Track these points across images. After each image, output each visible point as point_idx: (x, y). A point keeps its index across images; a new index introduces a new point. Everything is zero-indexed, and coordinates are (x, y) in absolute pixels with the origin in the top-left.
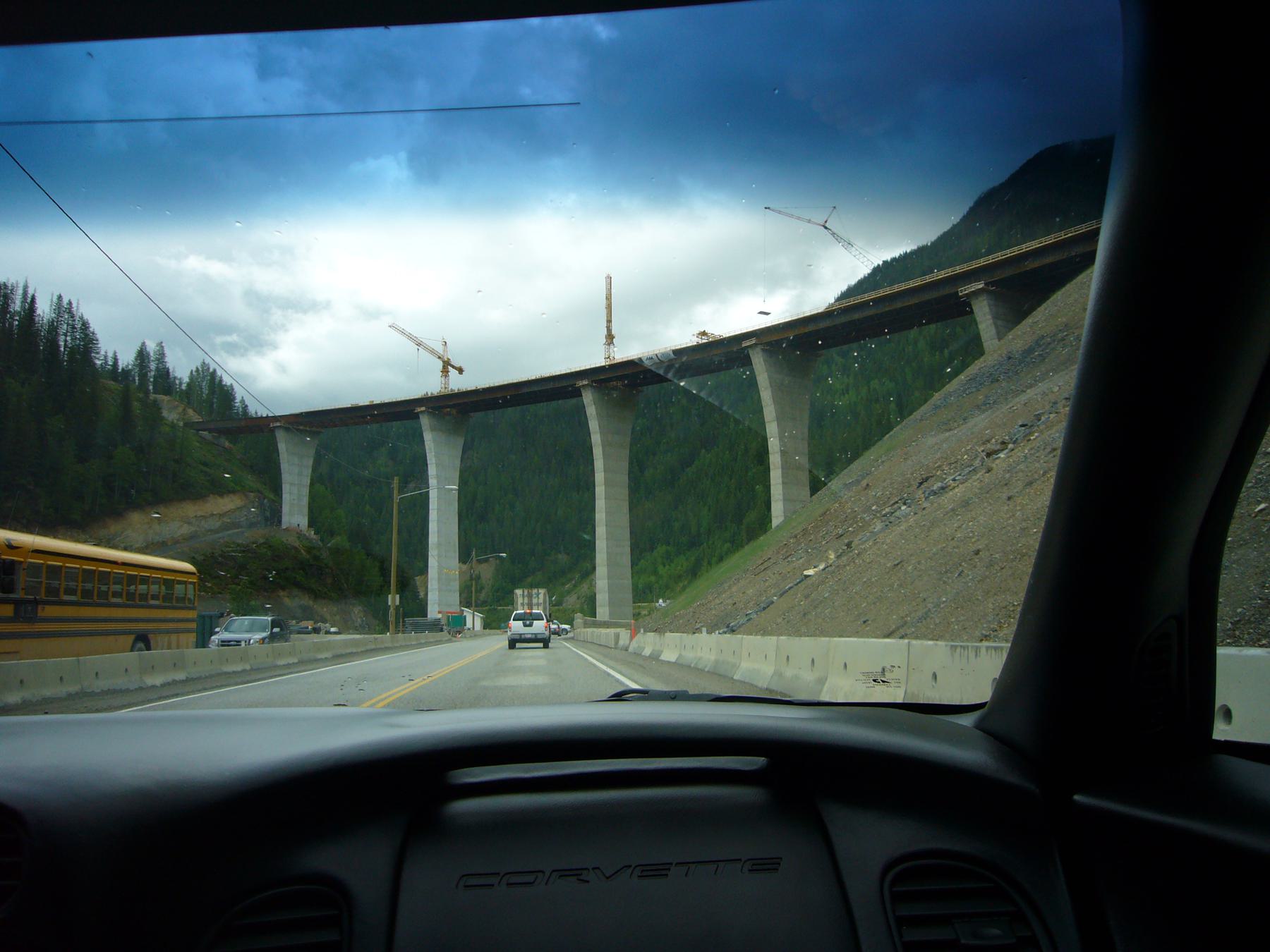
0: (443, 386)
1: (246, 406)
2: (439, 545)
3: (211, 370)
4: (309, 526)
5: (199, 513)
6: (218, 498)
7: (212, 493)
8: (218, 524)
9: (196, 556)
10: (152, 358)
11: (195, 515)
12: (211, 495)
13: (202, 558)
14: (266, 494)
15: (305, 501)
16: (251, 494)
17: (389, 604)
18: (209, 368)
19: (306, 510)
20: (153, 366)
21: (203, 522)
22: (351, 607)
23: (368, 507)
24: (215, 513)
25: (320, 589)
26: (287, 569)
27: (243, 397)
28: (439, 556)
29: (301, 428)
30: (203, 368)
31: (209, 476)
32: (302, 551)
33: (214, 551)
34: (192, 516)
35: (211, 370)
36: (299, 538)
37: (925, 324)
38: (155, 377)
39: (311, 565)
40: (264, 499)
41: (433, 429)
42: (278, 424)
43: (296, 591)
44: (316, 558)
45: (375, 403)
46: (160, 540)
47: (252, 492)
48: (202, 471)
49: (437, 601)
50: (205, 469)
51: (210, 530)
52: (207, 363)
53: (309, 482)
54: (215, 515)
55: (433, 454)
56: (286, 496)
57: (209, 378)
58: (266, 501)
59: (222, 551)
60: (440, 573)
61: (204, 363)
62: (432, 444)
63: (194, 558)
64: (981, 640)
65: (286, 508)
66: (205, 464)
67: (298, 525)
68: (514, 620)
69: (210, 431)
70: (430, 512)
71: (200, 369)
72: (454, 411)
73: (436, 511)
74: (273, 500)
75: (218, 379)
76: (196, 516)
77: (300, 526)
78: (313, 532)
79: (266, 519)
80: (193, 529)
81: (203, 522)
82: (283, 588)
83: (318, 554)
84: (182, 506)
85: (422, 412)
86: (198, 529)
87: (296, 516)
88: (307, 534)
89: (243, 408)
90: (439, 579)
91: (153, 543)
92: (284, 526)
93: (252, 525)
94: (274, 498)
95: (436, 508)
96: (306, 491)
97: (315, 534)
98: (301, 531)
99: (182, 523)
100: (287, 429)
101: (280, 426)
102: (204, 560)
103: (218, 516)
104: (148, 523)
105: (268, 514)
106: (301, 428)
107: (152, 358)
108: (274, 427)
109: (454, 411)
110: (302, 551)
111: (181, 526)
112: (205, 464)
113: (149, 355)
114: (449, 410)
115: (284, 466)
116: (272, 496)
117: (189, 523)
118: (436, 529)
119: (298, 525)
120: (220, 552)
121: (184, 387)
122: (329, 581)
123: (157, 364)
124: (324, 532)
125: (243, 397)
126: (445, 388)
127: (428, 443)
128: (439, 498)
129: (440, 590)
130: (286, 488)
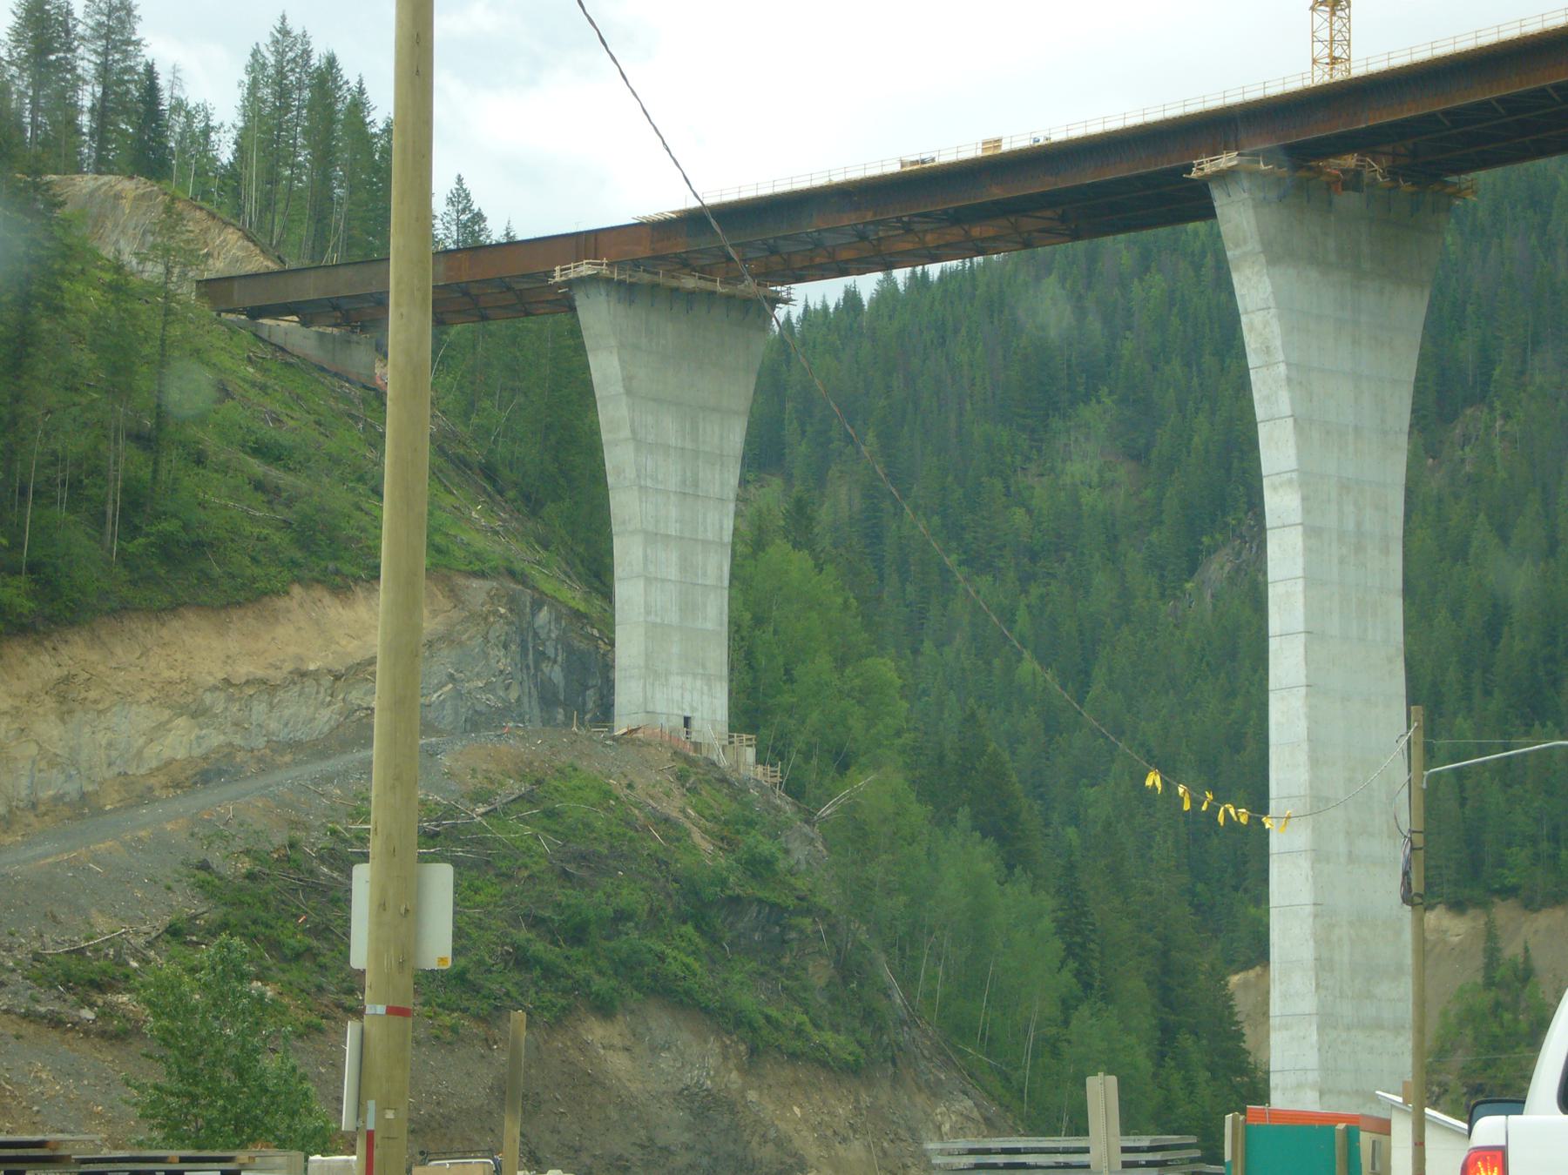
0: (1322, 51)
1: (478, 217)
2: (1318, 805)
3: (316, 61)
4: (732, 728)
5: (244, 670)
6: (327, 599)
7: (298, 580)
8: (325, 718)
9: (216, 858)
10: (80, 29)
11: (221, 675)
12: (297, 590)
13: (245, 865)
14: (548, 587)
15: (714, 613)
16: (475, 583)
17: (359, 956)
18: (306, 53)
19: (717, 656)
20: (86, 61)
21: (259, 708)
22: (920, 1099)
23: (1029, 666)
24: (312, 667)
25: (773, 1012)
26: (621, 916)
27: (460, 180)
28: (1319, 855)
29: (690, 282)
30: (280, 54)
31: (289, 503)
32: (697, 836)
33: (300, 835)
34: (211, 681)
35: (316, 61)
36: (681, 778)
37: (1340, 1118)
38: (102, 112)
39: (736, 900)
40: (537, 605)
41: (1276, 254)
42: (585, 269)
43: (660, 1022)
44: (758, 867)
45: (1006, 147)
46: (71, 789)
47: (481, 575)
48: (259, 486)
49: (1313, 1077)
50: (276, 474)
51: (295, 746)
52: (297, 31)
53: (729, 524)
54: (315, 675)
55: (1282, 368)
56: (628, 592)
57: (307, 94)
58: (544, 615)
59: (334, 832)
60: (1323, 939)
61: (285, 32)
62: (1276, 328)
63: (204, 866)
64: (1485, 1070)
65: (629, 649)
66: (262, 450)
67: (687, 721)
68: (372, 661)
69: (307, 312)
70: (1273, 644)
71: (271, 60)
72: (1376, 170)
73: (1301, 583)
74: (578, 615)
75: (345, 97)
76: (227, 681)
77: (695, 724)
78: (750, 754)
79: (548, 699)
80: (216, 739)
81: (259, 708)
82: (604, 1009)
83: (766, 847)
84: (164, 632)
85: (1223, 176)
86: (238, 740)
87: (676, 680)
88: (724, 762)
89: (462, 226)
90: (1323, 965)
91: (34, 806)
92: (618, 733)
93: (477, 722)
94: (582, 607)
95: (1300, 573)
96: (717, 567)
97: (760, 760)
98: (697, 746)
99: (167, 714)
100: (627, 291)
101: (593, 279)
102: (251, 876)
103: (327, 681)
104: (16, 713)
105: (556, 674)
106: (690, 282)
107: (80, 29)
108: (569, 283)
109: (1376, 170)
110: (697, 836)
111: (162, 727)
112: (262, 450)
113: (69, 13)
114: (1351, 161)
115: (619, 458)
116: (573, 596)
117: (198, 713)
118: (1301, 727)
119: (687, 721)
120: (326, 842)
121: (225, 151)
122: (819, 973)
123: (106, 53)
124: (807, 757)
125: (460, 180)
126: (1334, 60)
127: (1258, 318)
128: (1311, 580)
129: (1326, 1021)
130: (627, 553)
